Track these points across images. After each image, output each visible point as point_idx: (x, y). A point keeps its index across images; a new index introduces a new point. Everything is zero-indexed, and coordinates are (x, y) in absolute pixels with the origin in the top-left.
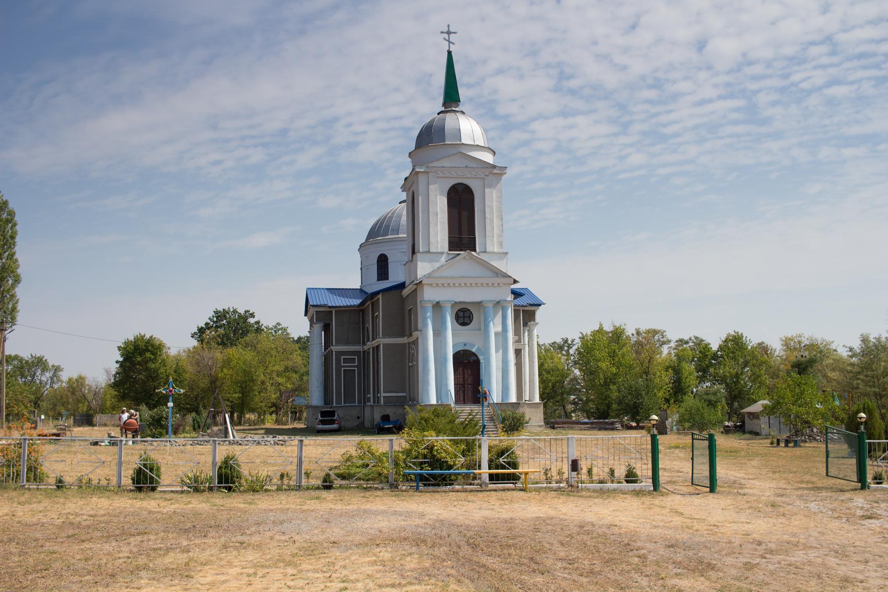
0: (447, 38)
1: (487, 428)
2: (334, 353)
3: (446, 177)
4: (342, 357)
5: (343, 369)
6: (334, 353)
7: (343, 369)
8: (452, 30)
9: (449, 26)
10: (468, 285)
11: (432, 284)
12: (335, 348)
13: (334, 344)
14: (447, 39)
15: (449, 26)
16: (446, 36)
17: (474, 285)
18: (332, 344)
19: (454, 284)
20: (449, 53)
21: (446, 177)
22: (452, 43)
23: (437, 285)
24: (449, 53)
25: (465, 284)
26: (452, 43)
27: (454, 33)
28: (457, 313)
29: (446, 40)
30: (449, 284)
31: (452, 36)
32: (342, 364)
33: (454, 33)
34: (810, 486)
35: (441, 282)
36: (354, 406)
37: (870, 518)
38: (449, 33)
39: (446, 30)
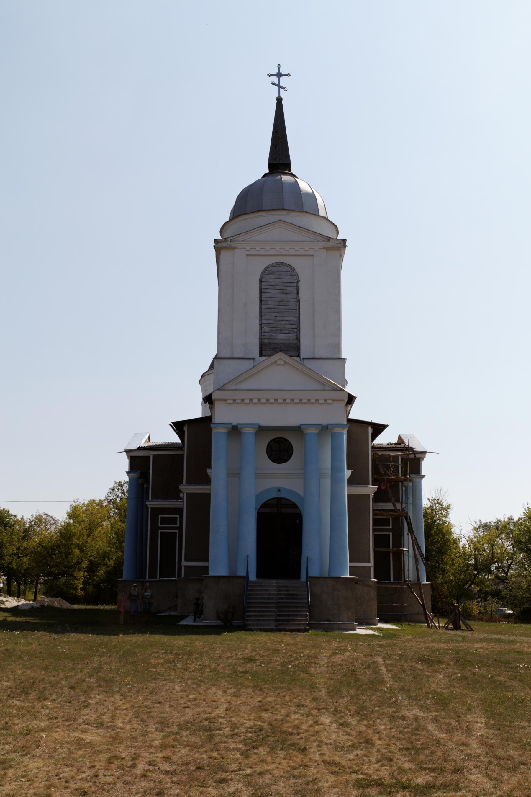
0: (277, 83)
1: (248, 611)
2: (150, 510)
3: (258, 255)
4: (160, 516)
5: (160, 531)
6: (150, 510)
7: (160, 531)
8: (283, 71)
9: (279, 67)
10: (272, 401)
11: (226, 400)
12: (152, 504)
13: (375, 533)
14: (277, 83)
15: (279, 67)
16: (275, 79)
17: (288, 401)
18: (148, 499)
19: (259, 400)
20: (279, 100)
21: (258, 255)
22: (284, 88)
23: (234, 400)
24: (279, 100)
25: (276, 400)
26: (284, 88)
27: (286, 75)
28: (269, 444)
29: (275, 84)
30: (251, 400)
31: (283, 79)
32: (160, 525)
33: (286, 75)
34: (322, 247)
35: (239, 396)
36: (156, 581)
37: (280, 279)
38: (279, 75)
39: (275, 71)
